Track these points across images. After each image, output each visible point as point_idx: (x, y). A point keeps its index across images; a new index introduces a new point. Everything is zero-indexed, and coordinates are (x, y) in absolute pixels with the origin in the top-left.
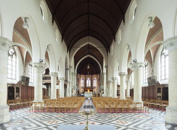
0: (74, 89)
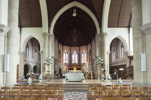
0: (48, 65)
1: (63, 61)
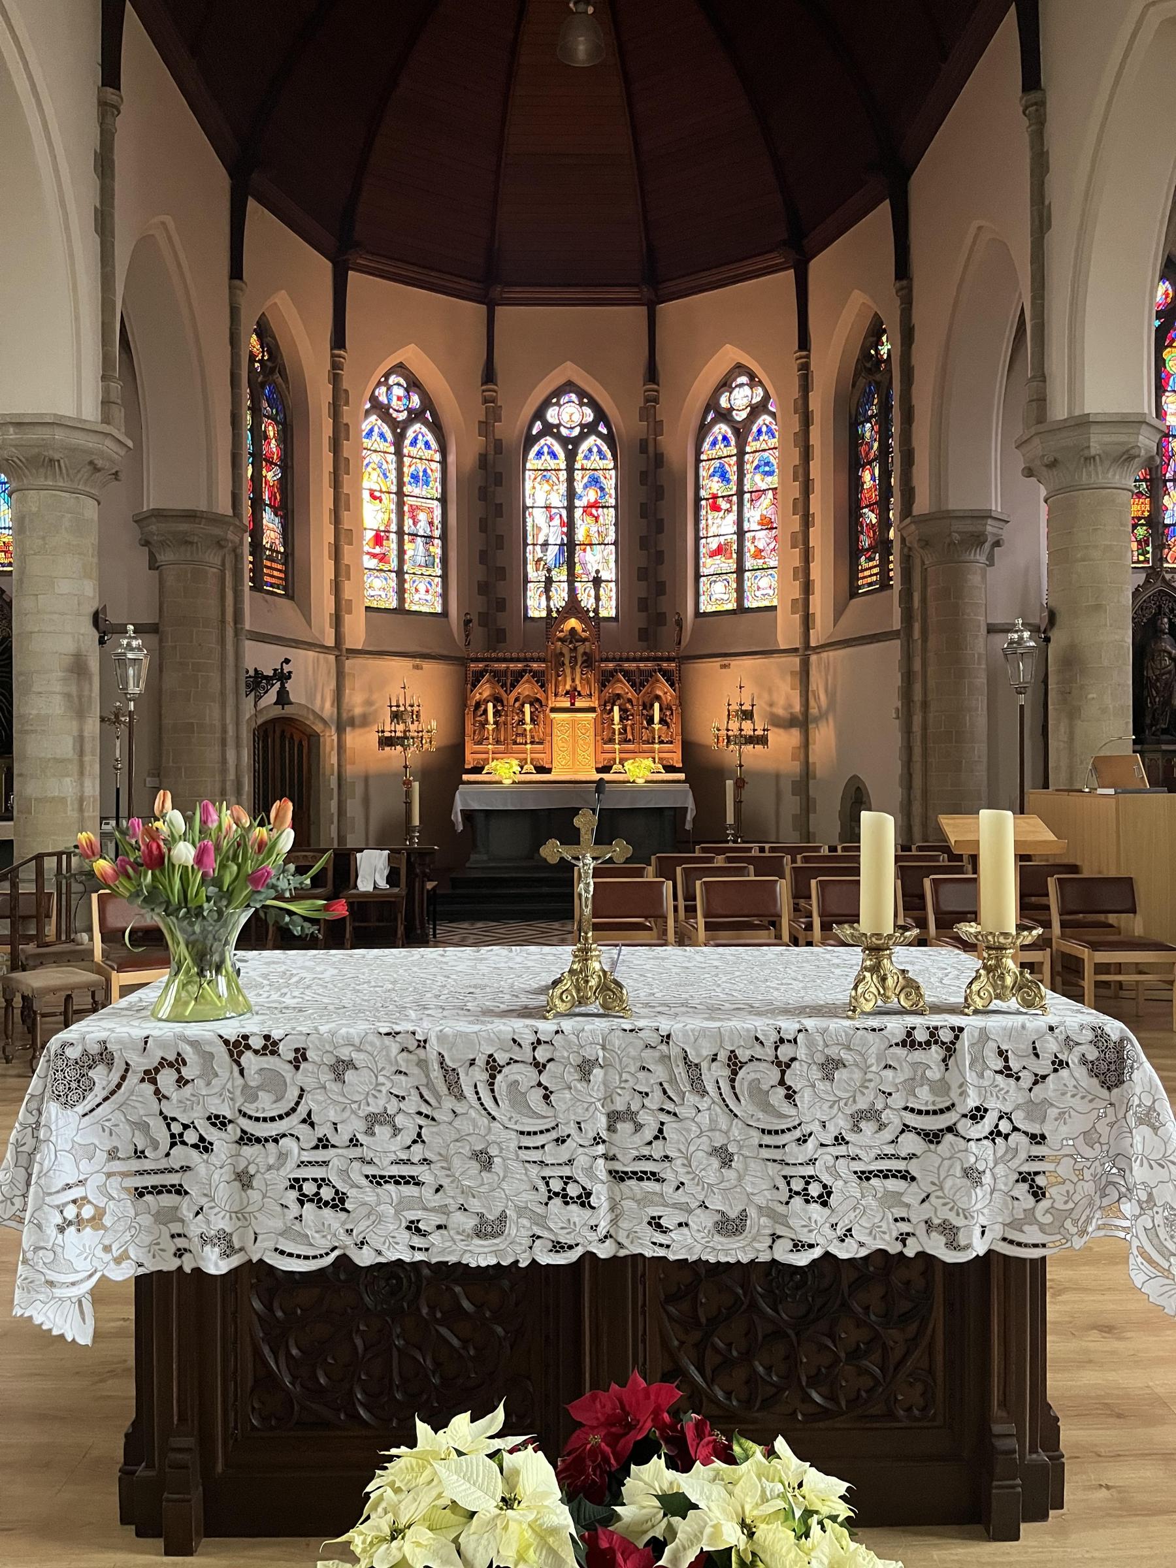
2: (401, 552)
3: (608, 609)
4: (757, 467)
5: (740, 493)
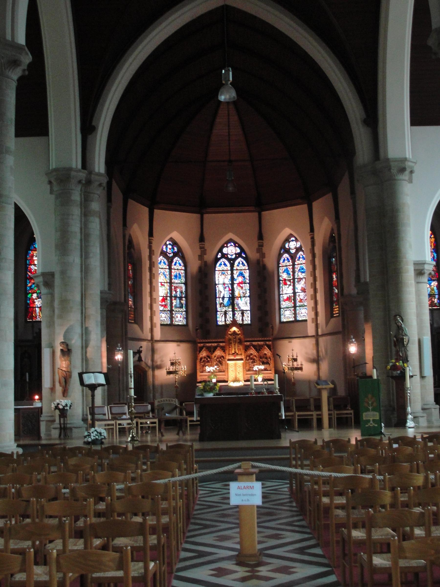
1: (152, 313)
2: (171, 303)
3: (247, 320)
4: (299, 270)
5: (294, 279)
